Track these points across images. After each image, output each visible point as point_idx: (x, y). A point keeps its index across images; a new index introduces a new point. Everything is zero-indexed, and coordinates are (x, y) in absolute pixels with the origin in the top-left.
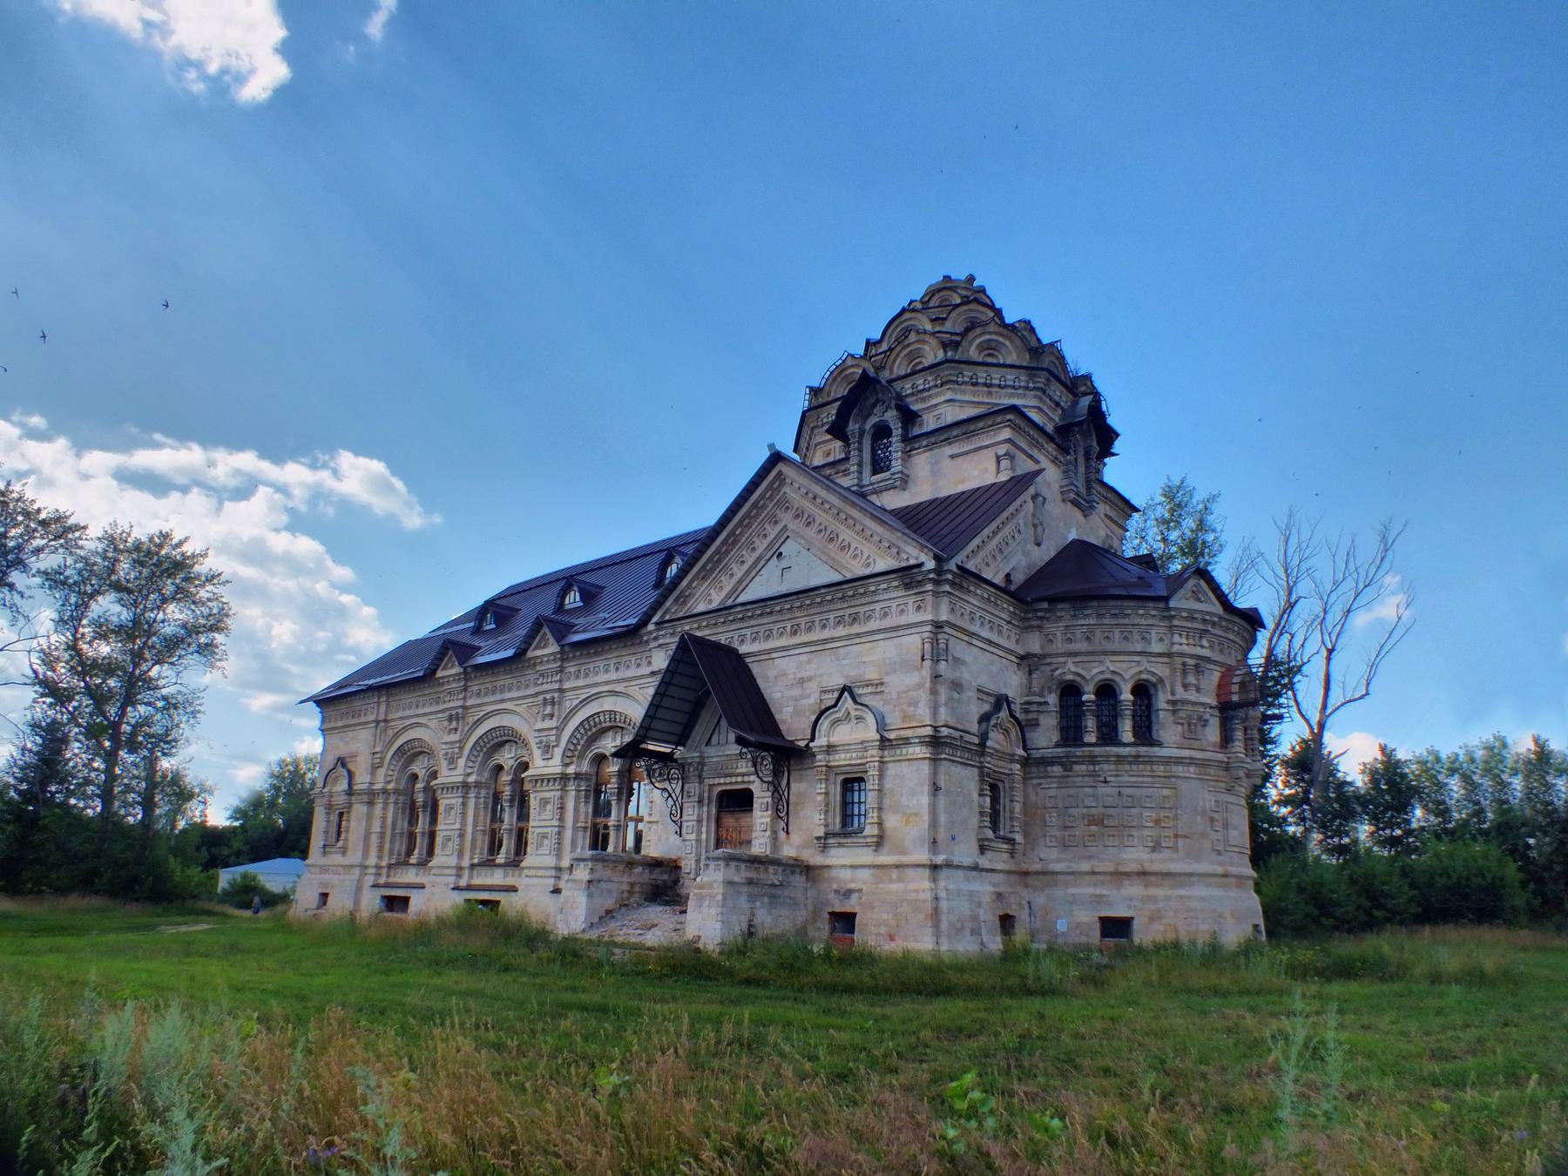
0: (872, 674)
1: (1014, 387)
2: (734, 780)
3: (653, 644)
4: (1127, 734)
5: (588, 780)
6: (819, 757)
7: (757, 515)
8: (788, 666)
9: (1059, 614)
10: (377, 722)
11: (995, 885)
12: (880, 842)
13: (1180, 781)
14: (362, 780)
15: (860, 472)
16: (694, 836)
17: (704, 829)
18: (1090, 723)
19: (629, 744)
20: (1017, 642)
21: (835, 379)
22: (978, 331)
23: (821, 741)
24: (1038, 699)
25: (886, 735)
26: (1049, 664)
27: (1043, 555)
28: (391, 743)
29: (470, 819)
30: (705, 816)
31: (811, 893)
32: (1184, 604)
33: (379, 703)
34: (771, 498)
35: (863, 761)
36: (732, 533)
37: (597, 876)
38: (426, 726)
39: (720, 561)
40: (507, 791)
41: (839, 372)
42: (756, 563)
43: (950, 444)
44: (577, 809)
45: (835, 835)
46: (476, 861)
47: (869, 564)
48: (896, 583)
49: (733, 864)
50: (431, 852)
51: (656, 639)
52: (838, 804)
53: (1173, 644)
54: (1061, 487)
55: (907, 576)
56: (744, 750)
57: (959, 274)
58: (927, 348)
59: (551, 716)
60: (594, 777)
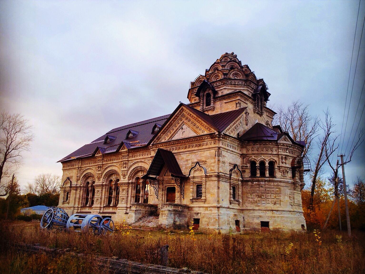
0: (204, 159)
1: (241, 85)
2: (171, 185)
3: (151, 150)
4: (267, 175)
5: (135, 184)
6: (191, 179)
7: (177, 118)
8: (184, 156)
9: (250, 144)
10: (79, 168)
11: (234, 213)
12: (205, 201)
13: (281, 187)
14: (74, 183)
15: (203, 106)
16: (161, 199)
17: (164, 197)
18: (258, 172)
19: (145, 176)
20: (240, 151)
21: (197, 81)
22: (232, 70)
23: (191, 175)
24: (245, 165)
25: (207, 174)
26: (248, 156)
27: (248, 128)
28: (82, 174)
29: (103, 194)
30: (164, 194)
31: (189, 213)
32: (282, 142)
33: (79, 163)
34: (180, 114)
35: (202, 181)
36: (171, 122)
37: (137, 209)
38: (92, 169)
39: (168, 129)
40: (113, 187)
41: (198, 79)
42: (176, 130)
43: (225, 99)
44: (131, 192)
45: (195, 199)
46: (105, 205)
47: (203, 132)
48: (209, 137)
49: (170, 206)
50: (92, 203)
51: (152, 148)
52: (196, 191)
53: (279, 152)
54: (254, 110)
55: (212, 136)
56: (173, 178)
57: (230, 52)
58: (220, 75)
59: (125, 167)
60: (136, 183)
